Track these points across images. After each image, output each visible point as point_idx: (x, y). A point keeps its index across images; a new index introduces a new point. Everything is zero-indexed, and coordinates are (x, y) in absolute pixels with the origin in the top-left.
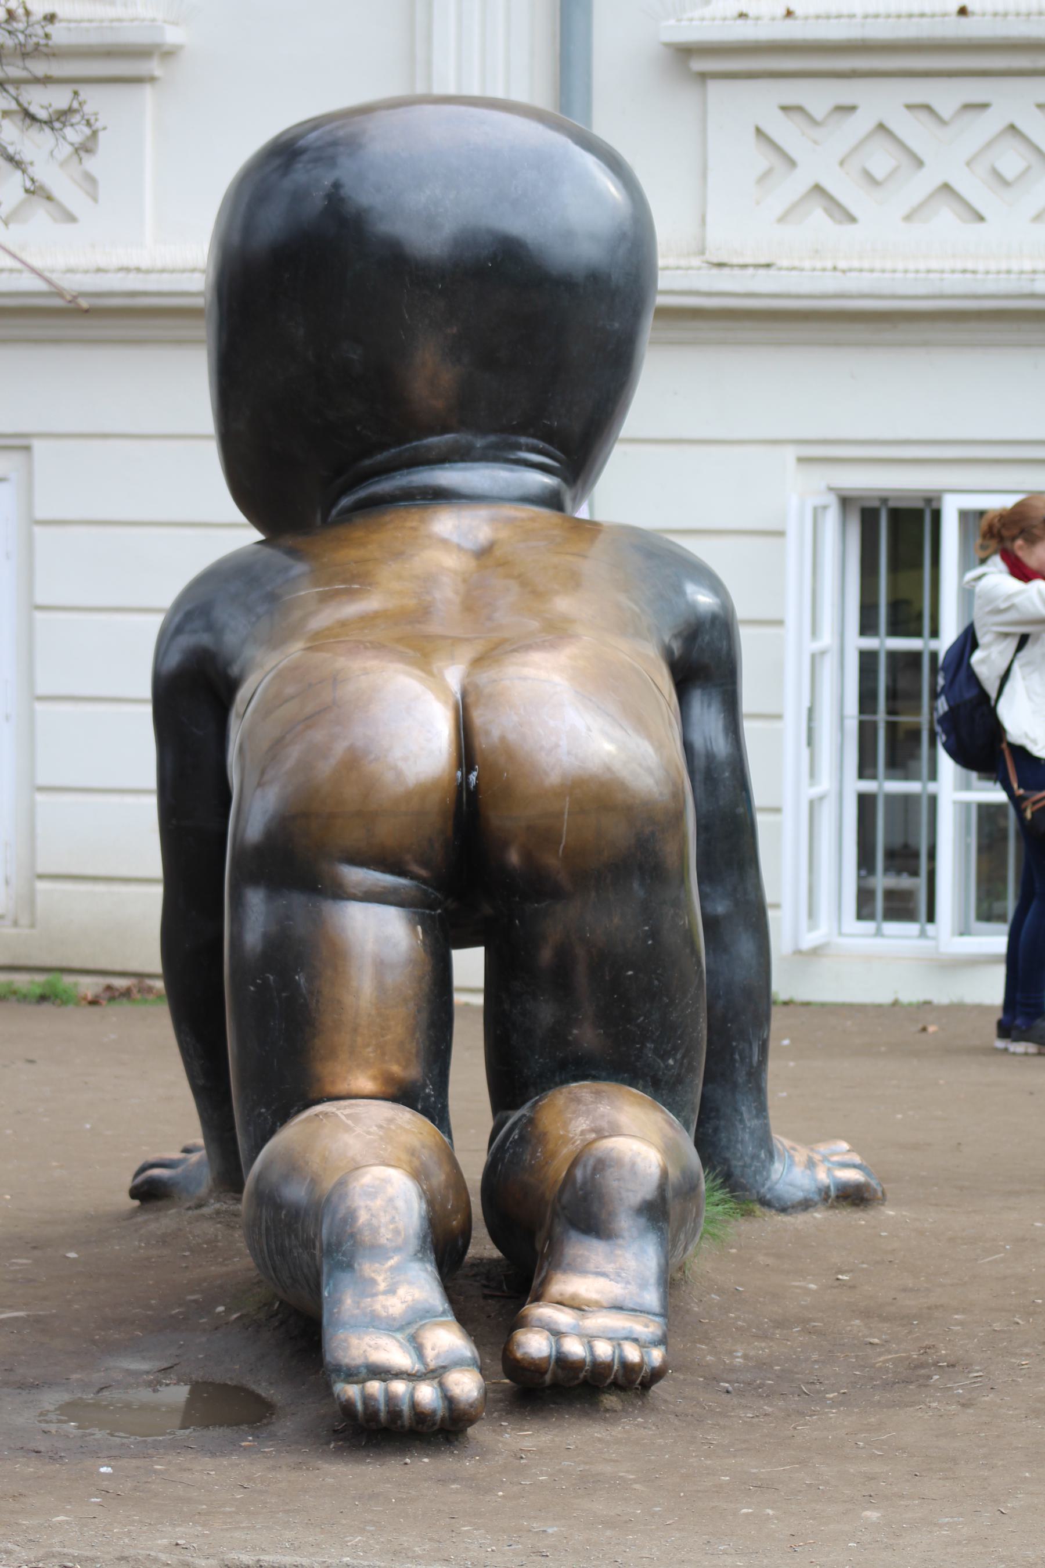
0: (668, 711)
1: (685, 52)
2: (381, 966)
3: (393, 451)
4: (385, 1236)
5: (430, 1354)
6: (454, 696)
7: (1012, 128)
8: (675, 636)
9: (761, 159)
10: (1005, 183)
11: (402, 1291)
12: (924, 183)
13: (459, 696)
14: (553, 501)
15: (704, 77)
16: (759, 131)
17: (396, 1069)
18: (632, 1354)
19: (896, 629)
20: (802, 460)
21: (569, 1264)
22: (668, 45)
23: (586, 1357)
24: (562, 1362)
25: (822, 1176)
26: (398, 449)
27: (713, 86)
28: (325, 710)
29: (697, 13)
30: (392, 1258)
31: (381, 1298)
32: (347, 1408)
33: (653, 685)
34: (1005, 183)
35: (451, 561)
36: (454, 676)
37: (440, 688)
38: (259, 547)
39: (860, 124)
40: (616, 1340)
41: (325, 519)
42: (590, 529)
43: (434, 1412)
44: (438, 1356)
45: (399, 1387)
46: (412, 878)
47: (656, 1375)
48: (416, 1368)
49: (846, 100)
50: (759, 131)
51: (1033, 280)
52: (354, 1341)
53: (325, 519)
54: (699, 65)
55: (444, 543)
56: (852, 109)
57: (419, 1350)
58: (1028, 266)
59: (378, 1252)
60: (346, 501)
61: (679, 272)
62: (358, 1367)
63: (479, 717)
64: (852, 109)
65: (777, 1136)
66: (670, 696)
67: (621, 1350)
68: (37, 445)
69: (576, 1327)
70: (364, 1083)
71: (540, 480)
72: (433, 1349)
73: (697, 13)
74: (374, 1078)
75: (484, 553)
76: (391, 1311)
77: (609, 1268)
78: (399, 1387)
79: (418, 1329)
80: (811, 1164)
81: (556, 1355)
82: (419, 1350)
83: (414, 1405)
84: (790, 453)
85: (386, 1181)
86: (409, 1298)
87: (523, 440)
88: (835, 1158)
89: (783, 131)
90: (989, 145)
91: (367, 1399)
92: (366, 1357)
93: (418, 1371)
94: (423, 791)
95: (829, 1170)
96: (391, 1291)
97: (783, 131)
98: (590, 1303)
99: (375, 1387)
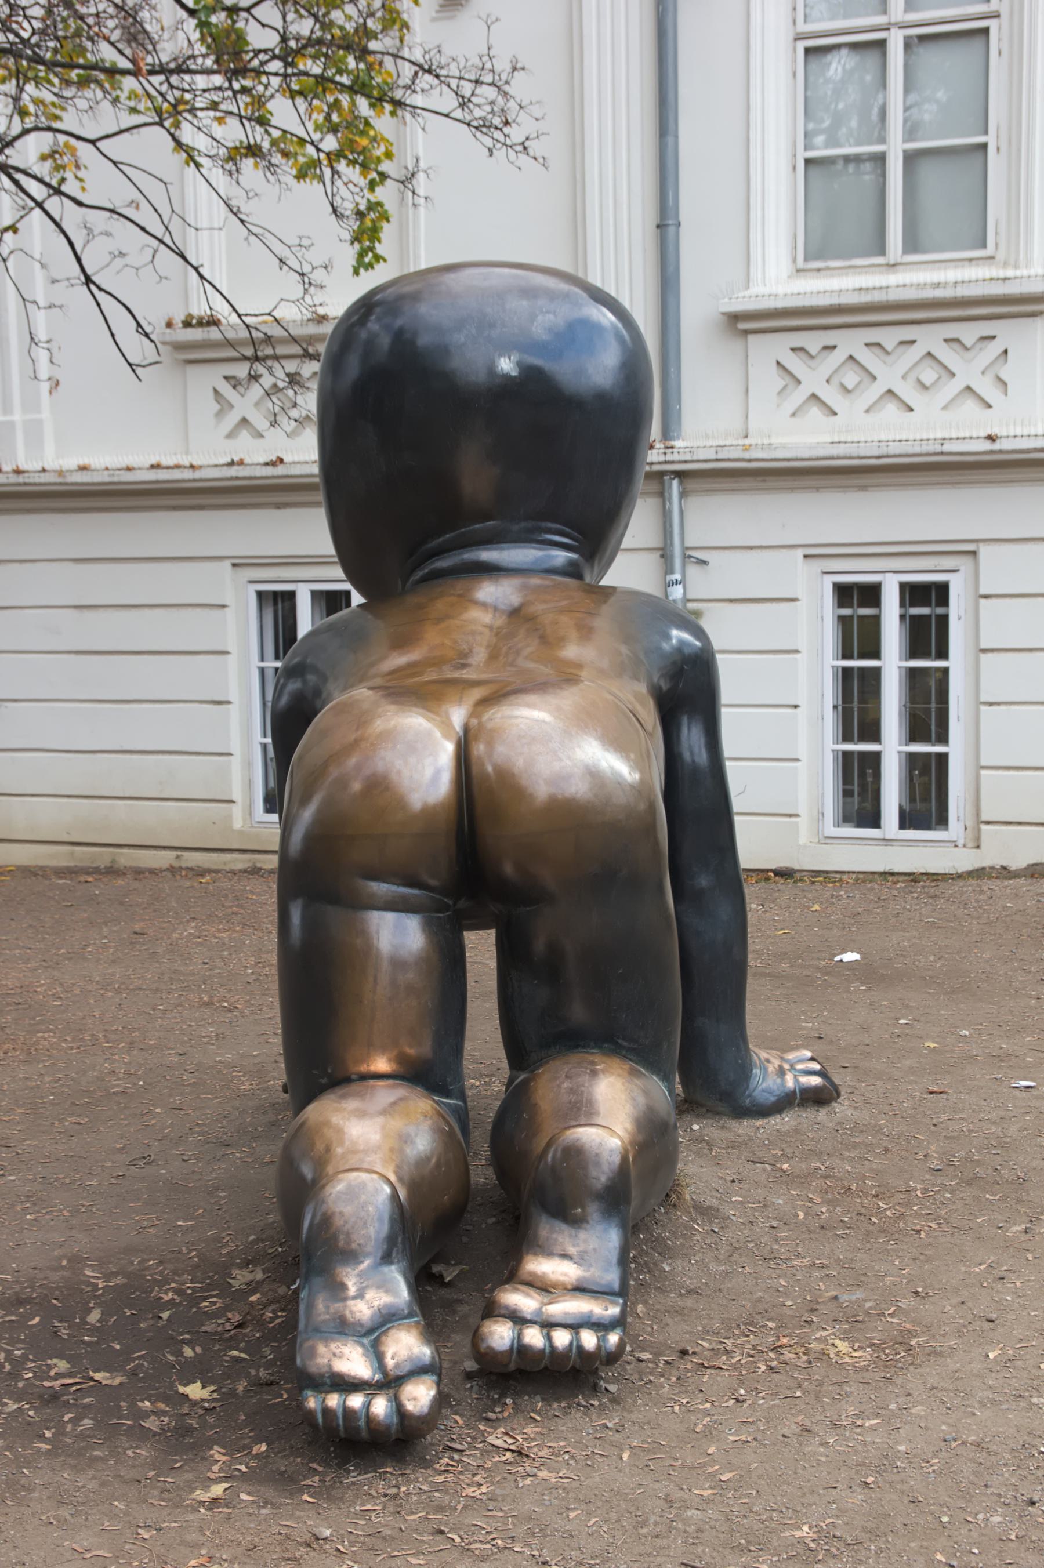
0: (646, 742)
1: (734, 318)
2: (398, 964)
3: (448, 536)
4: (358, 1239)
5: (390, 1363)
6: (458, 733)
7: (929, 354)
8: (662, 676)
9: (779, 381)
10: (925, 387)
11: (370, 1295)
12: (876, 390)
13: (461, 733)
14: (573, 571)
15: (746, 332)
16: (778, 363)
17: (411, 1051)
18: (589, 1340)
19: (862, 656)
20: (234, 565)
21: (539, 1246)
22: (723, 314)
23: (544, 1349)
24: (521, 1350)
25: (790, 1082)
26: (452, 535)
27: (751, 338)
28: (356, 742)
29: (741, 294)
30: (362, 1262)
31: (350, 1303)
32: (309, 1416)
33: (634, 719)
34: (925, 387)
35: (487, 618)
36: (458, 716)
37: (446, 725)
38: (358, 609)
39: (837, 357)
40: (575, 1327)
41: (404, 586)
42: (609, 592)
43: (388, 1427)
44: (397, 1366)
45: (356, 1401)
46: (424, 889)
47: (612, 1358)
48: (376, 1379)
49: (830, 343)
50: (778, 363)
51: (942, 444)
52: (321, 1349)
53: (404, 586)
54: (742, 326)
55: (484, 605)
56: (913, 342)
57: (378, 1357)
58: (939, 435)
59: (351, 1256)
60: (419, 574)
61: (732, 448)
62: (322, 1376)
63: (479, 749)
64: (913, 342)
65: (757, 1050)
66: (655, 727)
67: (578, 1340)
68: (984, 550)
69: (539, 1312)
70: (382, 1064)
71: (561, 557)
72: (393, 1358)
73: (741, 294)
74: (390, 1060)
75: (515, 613)
76: (358, 1316)
77: (572, 1250)
78: (356, 1401)
79: (379, 1337)
80: (781, 1072)
81: (517, 1348)
82: (378, 1357)
83: (369, 1418)
84: (800, 553)
85: (363, 1185)
86: (376, 1304)
87: (550, 525)
88: (799, 1067)
89: (794, 363)
90: (916, 365)
91: (327, 1411)
92: (330, 1366)
93: (377, 1381)
94: (429, 813)
95: (795, 1076)
96: (360, 1295)
97: (794, 363)
98: (555, 1285)
99: (333, 1400)
